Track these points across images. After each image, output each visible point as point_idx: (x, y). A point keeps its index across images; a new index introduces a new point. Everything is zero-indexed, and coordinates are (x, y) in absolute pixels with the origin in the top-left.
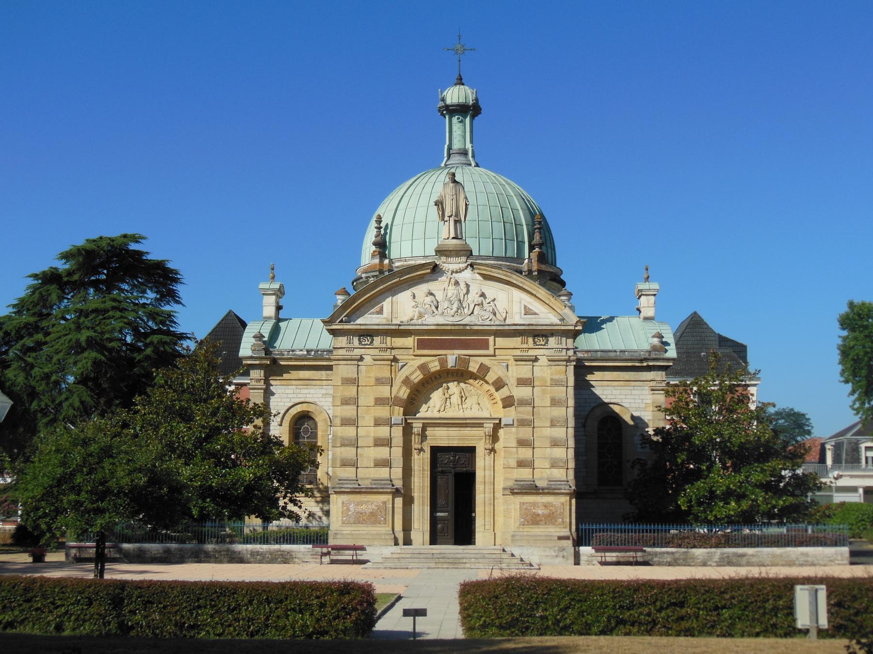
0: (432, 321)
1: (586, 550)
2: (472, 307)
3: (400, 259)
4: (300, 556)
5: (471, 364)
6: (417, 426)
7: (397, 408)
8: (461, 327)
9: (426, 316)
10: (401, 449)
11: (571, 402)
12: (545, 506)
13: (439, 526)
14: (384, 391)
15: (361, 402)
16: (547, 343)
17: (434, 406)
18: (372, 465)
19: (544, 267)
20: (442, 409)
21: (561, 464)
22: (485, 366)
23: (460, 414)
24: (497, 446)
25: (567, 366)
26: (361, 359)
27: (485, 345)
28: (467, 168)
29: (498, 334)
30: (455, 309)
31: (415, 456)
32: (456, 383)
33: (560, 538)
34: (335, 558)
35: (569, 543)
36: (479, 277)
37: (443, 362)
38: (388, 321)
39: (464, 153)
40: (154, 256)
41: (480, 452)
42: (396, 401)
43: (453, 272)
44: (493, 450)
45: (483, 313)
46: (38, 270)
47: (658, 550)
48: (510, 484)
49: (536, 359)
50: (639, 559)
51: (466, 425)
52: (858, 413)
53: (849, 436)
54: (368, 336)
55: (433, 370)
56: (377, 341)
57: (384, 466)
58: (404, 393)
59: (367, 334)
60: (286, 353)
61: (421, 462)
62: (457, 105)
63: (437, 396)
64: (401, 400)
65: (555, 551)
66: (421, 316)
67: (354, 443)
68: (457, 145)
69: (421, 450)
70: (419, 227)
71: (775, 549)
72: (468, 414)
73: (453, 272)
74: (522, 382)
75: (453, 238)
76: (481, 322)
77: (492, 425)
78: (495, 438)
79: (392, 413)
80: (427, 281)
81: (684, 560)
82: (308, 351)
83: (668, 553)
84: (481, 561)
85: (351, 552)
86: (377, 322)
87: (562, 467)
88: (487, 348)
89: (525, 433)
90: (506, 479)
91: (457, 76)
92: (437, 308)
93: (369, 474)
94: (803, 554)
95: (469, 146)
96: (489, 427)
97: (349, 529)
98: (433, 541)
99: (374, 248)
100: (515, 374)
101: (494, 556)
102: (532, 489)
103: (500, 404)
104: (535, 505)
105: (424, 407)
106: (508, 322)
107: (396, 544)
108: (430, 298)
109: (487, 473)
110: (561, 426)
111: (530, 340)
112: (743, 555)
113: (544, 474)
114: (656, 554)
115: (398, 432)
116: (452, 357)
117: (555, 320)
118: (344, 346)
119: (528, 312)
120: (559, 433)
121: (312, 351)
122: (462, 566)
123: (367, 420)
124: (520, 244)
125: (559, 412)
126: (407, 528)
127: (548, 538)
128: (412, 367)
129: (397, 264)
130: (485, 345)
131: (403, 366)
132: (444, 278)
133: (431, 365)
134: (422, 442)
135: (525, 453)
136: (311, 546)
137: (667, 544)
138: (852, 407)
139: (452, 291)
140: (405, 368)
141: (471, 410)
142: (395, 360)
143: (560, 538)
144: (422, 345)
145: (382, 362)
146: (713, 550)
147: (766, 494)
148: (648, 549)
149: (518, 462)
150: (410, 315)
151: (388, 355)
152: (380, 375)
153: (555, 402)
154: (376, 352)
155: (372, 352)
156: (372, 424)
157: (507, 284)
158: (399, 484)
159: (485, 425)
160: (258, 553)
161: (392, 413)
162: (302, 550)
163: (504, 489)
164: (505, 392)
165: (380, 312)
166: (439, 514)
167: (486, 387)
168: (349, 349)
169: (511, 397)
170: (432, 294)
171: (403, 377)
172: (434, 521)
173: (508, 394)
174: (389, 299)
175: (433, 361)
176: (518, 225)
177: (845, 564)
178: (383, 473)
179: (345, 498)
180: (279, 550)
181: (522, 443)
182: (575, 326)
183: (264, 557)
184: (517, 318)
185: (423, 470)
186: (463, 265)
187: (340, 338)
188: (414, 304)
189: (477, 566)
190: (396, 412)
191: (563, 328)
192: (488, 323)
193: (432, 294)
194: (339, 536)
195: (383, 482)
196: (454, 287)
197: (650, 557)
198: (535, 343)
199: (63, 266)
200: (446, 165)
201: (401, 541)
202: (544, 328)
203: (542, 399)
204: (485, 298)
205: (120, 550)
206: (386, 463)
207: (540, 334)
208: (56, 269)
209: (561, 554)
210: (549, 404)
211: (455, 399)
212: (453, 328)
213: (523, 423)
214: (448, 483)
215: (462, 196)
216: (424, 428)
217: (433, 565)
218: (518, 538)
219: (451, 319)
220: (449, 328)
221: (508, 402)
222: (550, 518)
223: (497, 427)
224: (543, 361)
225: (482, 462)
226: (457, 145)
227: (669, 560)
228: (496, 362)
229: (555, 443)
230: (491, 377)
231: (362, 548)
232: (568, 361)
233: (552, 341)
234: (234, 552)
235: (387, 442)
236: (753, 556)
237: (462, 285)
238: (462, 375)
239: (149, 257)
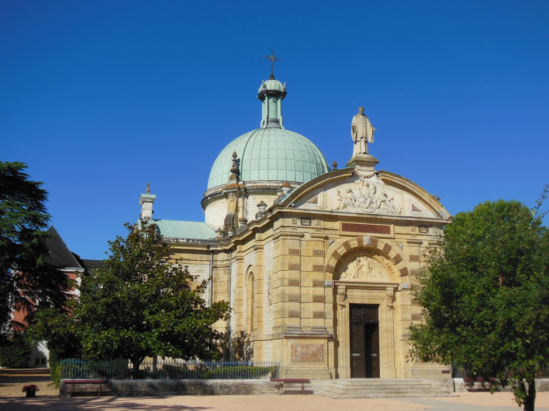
0: (352, 211)
3: (250, 182)
5: (379, 244)
8: (374, 217)
9: (349, 207)
14: (320, 261)
15: (303, 268)
17: (351, 274)
18: (312, 316)
20: (356, 277)
24: (395, 304)
26: (303, 236)
27: (387, 230)
30: (368, 204)
32: (365, 257)
33: (444, 372)
34: (287, 389)
35: (450, 375)
36: (382, 182)
37: (360, 241)
38: (321, 208)
39: (277, 121)
40: (32, 178)
42: (328, 269)
43: (365, 177)
51: (374, 288)
54: (307, 219)
55: (352, 247)
56: (314, 223)
58: (333, 263)
59: (307, 217)
60: (172, 240)
61: (344, 314)
63: (352, 267)
64: (332, 267)
65: (441, 382)
66: (345, 206)
67: (296, 299)
68: (272, 116)
69: (344, 306)
75: (364, 153)
76: (386, 214)
78: (393, 299)
80: (348, 182)
82: (187, 240)
85: (300, 385)
86: (314, 209)
88: (389, 233)
93: (310, 323)
95: (280, 117)
99: (231, 174)
100: (408, 253)
103: (399, 274)
105: (343, 275)
106: (402, 215)
107: (331, 378)
115: (329, 292)
116: (367, 238)
118: (290, 225)
119: (414, 209)
121: (190, 240)
122: (404, 395)
123: (308, 281)
127: (436, 372)
128: (339, 244)
129: (248, 185)
130: (387, 230)
131: (332, 243)
132: (359, 181)
133: (351, 243)
134: (344, 300)
139: (365, 190)
140: (333, 244)
143: (444, 372)
144: (345, 228)
145: (318, 239)
149: (412, 316)
150: (338, 206)
152: (317, 248)
155: (310, 231)
156: (311, 285)
157: (401, 189)
158: (331, 331)
159: (387, 289)
160: (226, 386)
162: (260, 383)
164: (401, 265)
165: (315, 202)
167: (386, 261)
171: (333, 251)
174: (322, 193)
175: (353, 240)
176: (323, 167)
179: (293, 341)
180: (242, 384)
182: (448, 221)
183: (230, 390)
184: (408, 213)
186: (372, 173)
187: (287, 219)
188: (339, 198)
190: (328, 276)
194: (289, 372)
195: (321, 330)
196: (366, 188)
198: (420, 231)
201: (334, 376)
204: (387, 197)
205: (110, 385)
206: (320, 315)
207: (423, 224)
209: (445, 384)
211: (365, 269)
212: (368, 216)
219: (366, 210)
220: (366, 216)
225: (383, 316)
228: (394, 243)
230: (392, 254)
231: (307, 381)
234: (207, 386)
237: (371, 187)
238: (370, 252)
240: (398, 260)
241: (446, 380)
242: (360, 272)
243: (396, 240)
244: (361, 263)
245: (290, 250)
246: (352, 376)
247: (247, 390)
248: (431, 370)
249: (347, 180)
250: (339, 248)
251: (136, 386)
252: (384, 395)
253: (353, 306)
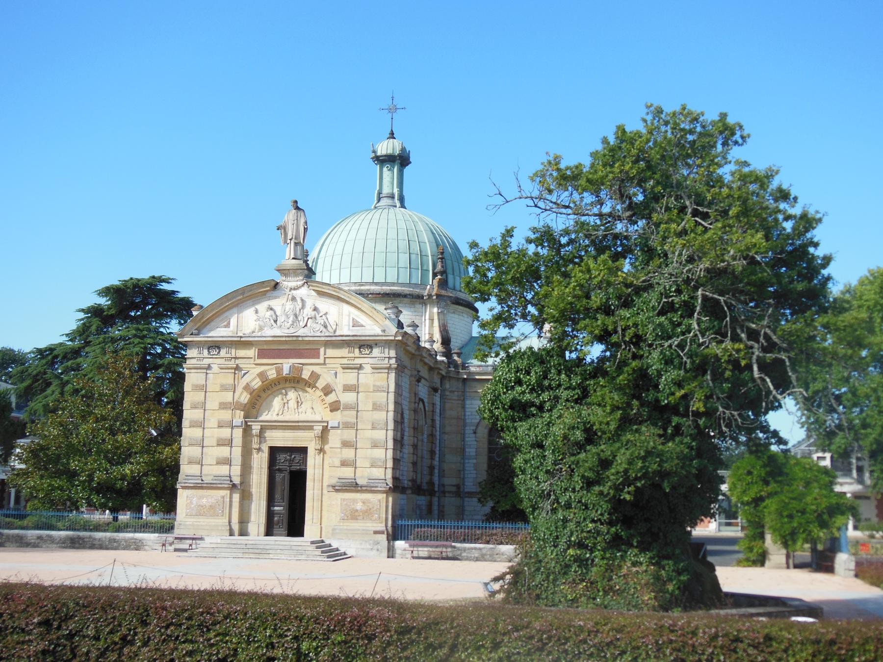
0: (271, 332)
1: (400, 544)
2: (306, 319)
4: (150, 543)
6: (256, 428)
7: (238, 412)
8: (295, 339)
10: (240, 449)
11: (391, 407)
12: (364, 503)
13: (276, 519)
14: (228, 397)
16: (371, 352)
17: (278, 409)
19: (443, 292)
21: (380, 464)
22: (316, 373)
23: (296, 418)
26: (209, 367)
28: (392, 210)
29: (331, 344)
30: (290, 322)
31: (255, 456)
33: (376, 532)
35: (384, 537)
36: (314, 293)
37: (279, 370)
41: (311, 452)
43: (291, 289)
44: (321, 451)
45: (315, 325)
46: (84, 306)
48: (334, 481)
49: (360, 368)
50: (450, 555)
52: (803, 427)
53: (803, 447)
57: (224, 464)
58: (245, 398)
59: (215, 346)
61: (260, 462)
62: (385, 156)
63: (277, 402)
64: (241, 404)
66: (261, 328)
68: (386, 190)
69: (259, 450)
70: (337, 259)
72: (302, 417)
73: (291, 289)
74: (347, 388)
76: (312, 334)
77: (259, 427)
79: (233, 416)
81: (491, 555)
83: (475, 549)
84: (286, 552)
87: (380, 467)
88: (318, 358)
89: (349, 435)
90: (330, 477)
91: (389, 131)
92: (275, 321)
93: (212, 471)
96: (318, 428)
98: (269, 532)
101: (300, 548)
102: (353, 486)
104: (355, 501)
106: (338, 333)
107: (231, 534)
108: (270, 313)
109: (317, 471)
110: (382, 429)
111: (357, 350)
112: (115, 540)
113: (363, 475)
114: (465, 549)
115: (238, 433)
116: (287, 365)
117: (378, 331)
119: (356, 324)
120: (380, 435)
122: (267, 556)
124: (424, 272)
125: (380, 416)
126: (244, 521)
131: (245, 374)
135: (349, 453)
136: (157, 535)
137: (476, 541)
138: (798, 422)
139: (289, 306)
141: (305, 414)
142: (237, 368)
143: (376, 532)
147: (98, 496)
148: (458, 545)
151: (232, 364)
152: (224, 382)
153: (376, 407)
154: (222, 361)
158: (237, 480)
161: (233, 416)
163: (328, 486)
164: (332, 398)
165: (228, 326)
166: (276, 508)
168: (199, 359)
169: (337, 402)
170: (271, 309)
171: (245, 384)
172: (270, 515)
173: (335, 399)
176: (422, 255)
178: (224, 470)
180: (133, 539)
181: (346, 444)
183: (119, 545)
184: (346, 330)
185: (261, 468)
186: (301, 283)
189: (279, 557)
190: (237, 416)
191: (384, 338)
192: (319, 334)
193: (271, 309)
197: (459, 552)
199: (103, 301)
200: (375, 208)
201: (236, 532)
202: (367, 338)
203: (365, 404)
206: (228, 462)
207: (365, 344)
208: (99, 305)
209: (376, 547)
210: (370, 408)
211: (292, 404)
212: (287, 339)
213: (347, 426)
214: (282, 479)
215: (302, 221)
216: (262, 430)
217: (240, 555)
219: (287, 331)
220: (284, 339)
221: (335, 407)
222: (367, 514)
223: (325, 430)
224: (368, 369)
226: (386, 190)
227: (476, 555)
228: (326, 370)
229: (375, 445)
230: (321, 384)
232: (389, 368)
233: (376, 352)
235: (229, 443)
239: (180, 295)
240: (327, 390)
242: (286, 408)
243: (328, 366)
244: (288, 397)
245: (193, 385)
247: (137, 546)
249: (268, 294)
250: (253, 380)
251: (26, 536)
252: (234, 555)
253: (274, 451)
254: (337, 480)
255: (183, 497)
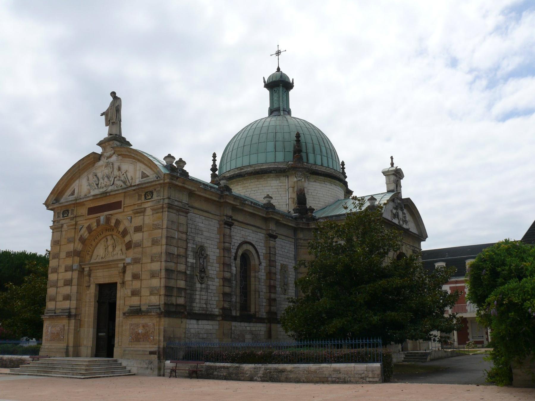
25: (163, 212)
33: (151, 353)
47: (218, 364)
48: (126, 309)
61: (92, 292)
65: (146, 364)
71: (353, 365)
83: (224, 367)
94: (335, 370)
97: (48, 344)
112: (283, 371)
114: (216, 368)
115: (76, 274)
135: (136, 284)
146: (260, 365)
155: (67, 221)
174: (77, 182)
177: (376, 382)
206: (67, 298)
209: (150, 366)
218: (127, 352)
223: (124, 268)
224: (149, 212)
227: (225, 374)
229: (153, 275)
232: (163, 208)
236: (291, 371)
241: (151, 363)
246: (96, 356)
248: (140, 351)
254: (128, 308)
255: (48, 328)
